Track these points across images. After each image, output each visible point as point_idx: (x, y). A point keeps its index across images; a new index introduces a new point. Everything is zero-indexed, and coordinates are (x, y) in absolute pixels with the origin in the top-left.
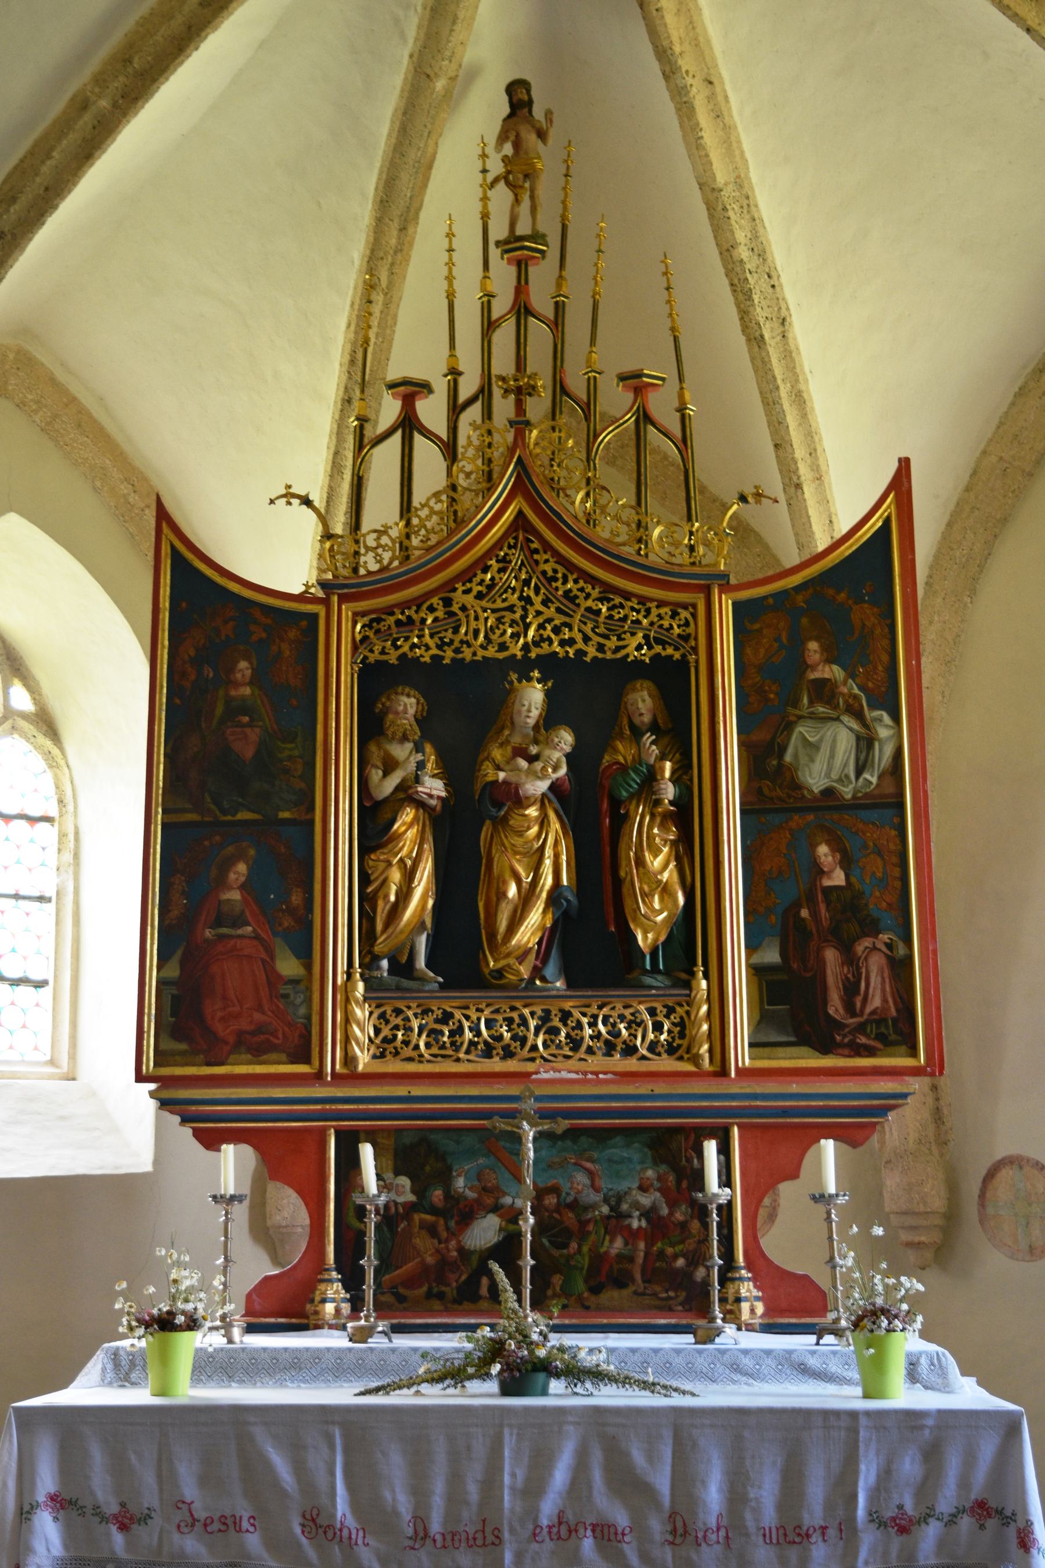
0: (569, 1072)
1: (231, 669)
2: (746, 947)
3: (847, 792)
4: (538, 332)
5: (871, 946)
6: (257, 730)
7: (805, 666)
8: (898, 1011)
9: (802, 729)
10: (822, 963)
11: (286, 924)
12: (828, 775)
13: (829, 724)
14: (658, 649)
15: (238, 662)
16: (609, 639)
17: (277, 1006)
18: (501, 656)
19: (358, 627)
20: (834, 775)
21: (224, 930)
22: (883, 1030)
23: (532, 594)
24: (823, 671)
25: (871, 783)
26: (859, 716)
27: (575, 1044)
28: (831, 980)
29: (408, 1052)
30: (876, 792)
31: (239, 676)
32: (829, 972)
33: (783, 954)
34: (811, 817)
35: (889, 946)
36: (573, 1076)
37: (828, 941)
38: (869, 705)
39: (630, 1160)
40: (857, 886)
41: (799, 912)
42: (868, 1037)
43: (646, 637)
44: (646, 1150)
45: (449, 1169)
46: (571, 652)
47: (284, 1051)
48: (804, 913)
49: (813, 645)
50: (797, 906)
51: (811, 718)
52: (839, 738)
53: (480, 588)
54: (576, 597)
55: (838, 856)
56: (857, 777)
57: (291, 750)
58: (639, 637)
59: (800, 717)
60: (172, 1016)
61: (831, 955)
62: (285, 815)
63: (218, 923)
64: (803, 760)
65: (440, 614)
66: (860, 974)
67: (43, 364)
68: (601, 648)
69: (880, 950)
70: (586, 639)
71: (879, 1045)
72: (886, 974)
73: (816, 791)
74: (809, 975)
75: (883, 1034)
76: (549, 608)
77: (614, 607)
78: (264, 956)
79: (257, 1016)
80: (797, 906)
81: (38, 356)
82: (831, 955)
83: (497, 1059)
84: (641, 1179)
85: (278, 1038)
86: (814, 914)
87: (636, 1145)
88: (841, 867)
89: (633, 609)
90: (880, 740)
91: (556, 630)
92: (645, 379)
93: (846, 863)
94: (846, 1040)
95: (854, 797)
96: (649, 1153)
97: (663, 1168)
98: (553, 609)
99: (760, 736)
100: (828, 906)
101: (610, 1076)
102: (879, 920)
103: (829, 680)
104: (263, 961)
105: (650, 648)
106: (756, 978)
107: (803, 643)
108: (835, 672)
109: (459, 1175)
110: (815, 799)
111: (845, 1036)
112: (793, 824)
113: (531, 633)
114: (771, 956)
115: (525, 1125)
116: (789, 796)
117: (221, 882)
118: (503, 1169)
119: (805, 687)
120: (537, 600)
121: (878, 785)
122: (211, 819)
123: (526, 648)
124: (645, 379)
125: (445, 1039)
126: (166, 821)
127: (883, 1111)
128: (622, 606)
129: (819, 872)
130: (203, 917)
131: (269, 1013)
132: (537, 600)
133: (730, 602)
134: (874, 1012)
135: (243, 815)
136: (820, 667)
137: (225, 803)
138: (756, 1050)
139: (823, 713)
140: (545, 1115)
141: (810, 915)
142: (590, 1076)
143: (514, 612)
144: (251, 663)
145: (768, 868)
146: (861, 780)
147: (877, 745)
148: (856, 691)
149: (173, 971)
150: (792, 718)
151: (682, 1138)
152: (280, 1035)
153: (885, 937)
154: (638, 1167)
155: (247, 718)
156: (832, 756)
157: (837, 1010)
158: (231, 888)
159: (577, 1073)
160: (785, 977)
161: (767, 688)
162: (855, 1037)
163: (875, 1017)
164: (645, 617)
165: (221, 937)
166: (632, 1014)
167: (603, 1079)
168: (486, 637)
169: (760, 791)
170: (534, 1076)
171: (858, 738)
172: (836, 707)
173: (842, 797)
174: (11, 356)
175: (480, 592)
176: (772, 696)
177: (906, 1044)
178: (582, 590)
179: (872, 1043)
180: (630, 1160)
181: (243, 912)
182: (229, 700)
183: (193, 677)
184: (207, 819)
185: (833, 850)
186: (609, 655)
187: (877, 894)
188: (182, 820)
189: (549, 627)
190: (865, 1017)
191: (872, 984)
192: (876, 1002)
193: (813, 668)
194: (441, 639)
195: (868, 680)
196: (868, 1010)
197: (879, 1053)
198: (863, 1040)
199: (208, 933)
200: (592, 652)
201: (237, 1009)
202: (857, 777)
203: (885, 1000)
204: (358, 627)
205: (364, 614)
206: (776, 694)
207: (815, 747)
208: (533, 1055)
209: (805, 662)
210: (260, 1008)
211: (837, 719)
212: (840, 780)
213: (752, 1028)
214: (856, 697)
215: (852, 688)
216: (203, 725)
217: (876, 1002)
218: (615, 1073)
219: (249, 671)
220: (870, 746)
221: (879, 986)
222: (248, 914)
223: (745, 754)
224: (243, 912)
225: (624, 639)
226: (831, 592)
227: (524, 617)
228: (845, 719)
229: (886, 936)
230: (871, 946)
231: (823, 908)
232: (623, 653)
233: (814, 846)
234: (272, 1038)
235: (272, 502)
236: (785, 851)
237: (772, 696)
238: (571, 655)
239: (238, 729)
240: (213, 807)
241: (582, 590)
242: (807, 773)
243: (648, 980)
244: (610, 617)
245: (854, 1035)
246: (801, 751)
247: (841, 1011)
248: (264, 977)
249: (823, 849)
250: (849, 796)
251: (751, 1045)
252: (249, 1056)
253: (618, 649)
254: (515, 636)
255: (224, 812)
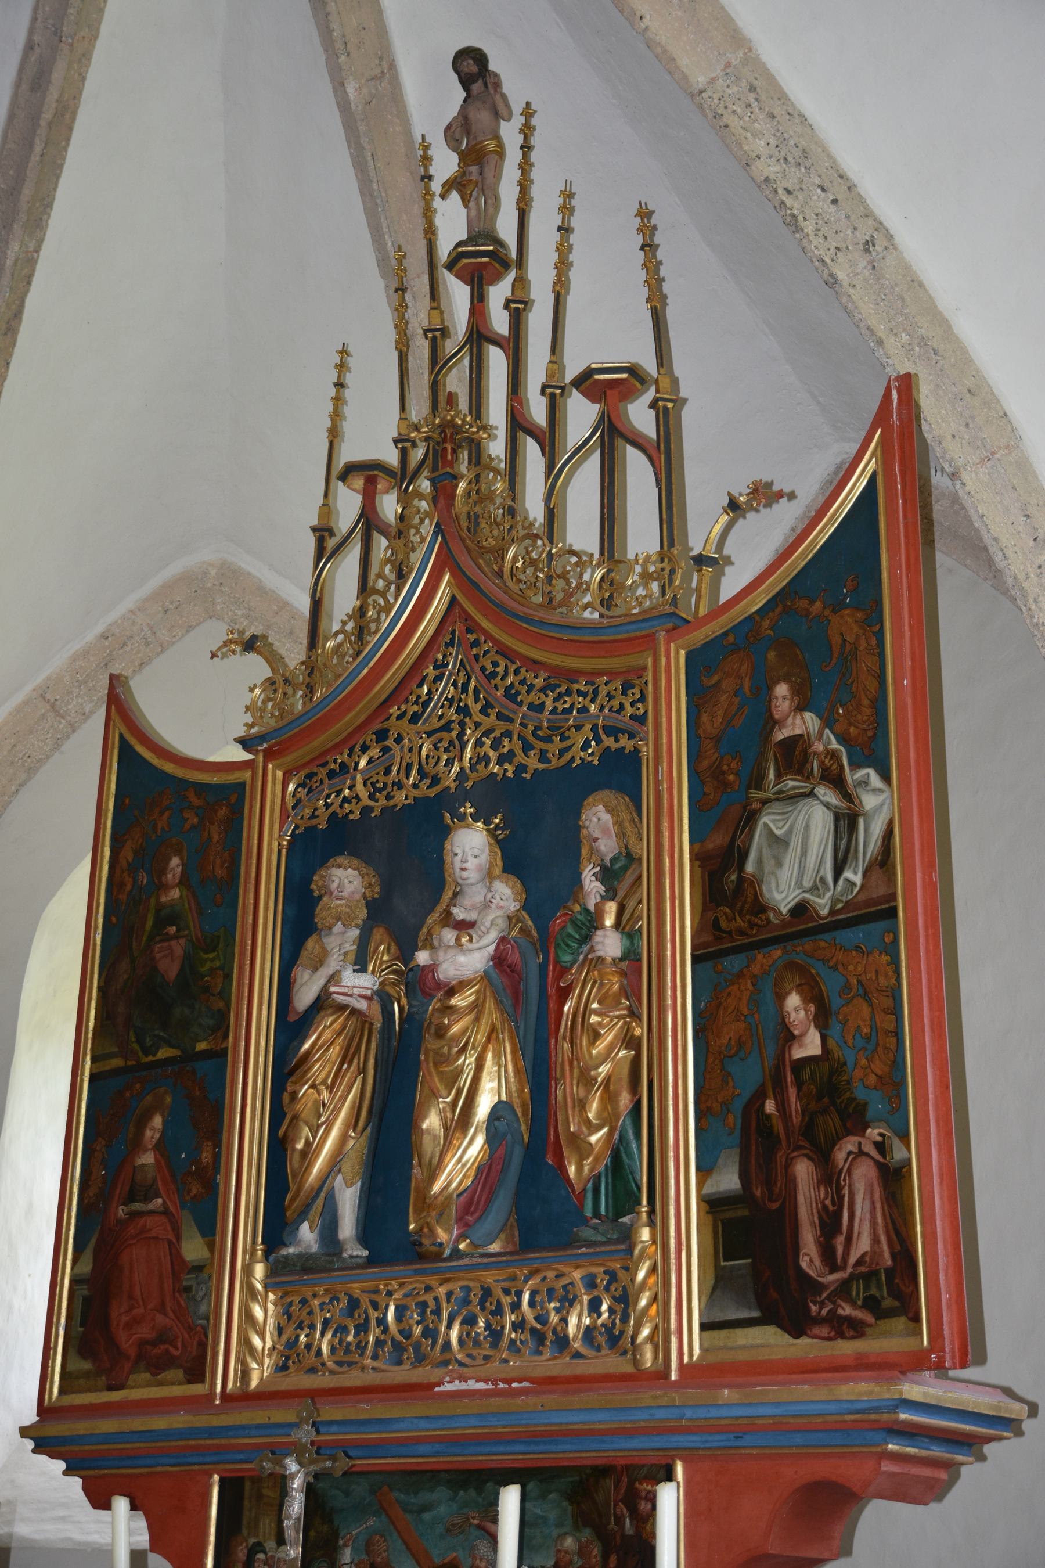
0: (478, 1381)
1: (163, 871)
2: (698, 1169)
3: (823, 904)
4: (497, 360)
5: (855, 1149)
6: (182, 941)
7: (772, 723)
8: (893, 1256)
9: (769, 820)
10: (791, 1183)
11: (194, 1191)
12: (799, 884)
13: (801, 804)
14: (609, 742)
15: (171, 859)
16: (552, 742)
17: (179, 1304)
18: (432, 793)
19: (291, 787)
20: (807, 883)
21: (137, 1206)
22: (874, 1291)
23: (470, 701)
24: (793, 724)
25: (854, 884)
26: (837, 782)
27: (495, 1334)
28: (803, 1212)
29: (311, 1359)
30: (860, 898)
31: (170, 876)
32: (801, 1199)
33: (744, 1176)
34: (777, 952)
35: (881, 1147)
36: (481, 1385)
37: (800, 1148)
38: (850, 764)
39: (545, 1519)
40: (837, 1053)
41: (763, 1104)
42: (853, 1303)
43: (594, 728)
44: (565, 1504)
45: (335, 1534)
46: (510, 769)
47: (181, 1366)
48: (770, 1106)
49: (782, 690)
50: (760, 1096)
51: (777, 799)
52: (813, 823)
53: (415, 708)
54: (518, 693)
55: (812, 1008)
56: (836, 879)
57: (212, 960)
58: (587, 731)
59: (765, 802)
60: (80, 1327)
61: (803, 1170)
62: (202, 1046)
63: (131, 1198)
64: (769, 864)
65: (375, 752)
66: (841, 1198)
67: (249, 574)
68: (543, 757)
69: (867, 1155)
70: (527, 748)
71: (869, 1318)
72: (877, 1195)
73: (784, 911)
74: (775, 1206)
75: (872, 1298)
76: (488, 716)
77: (560, 696)
78: (171, 1236)
79: (160, 1318)
80: (760, 1096)
81: (243, 566)
82: (803, 1170)
83: (406, 1366)
84: (559, 1551)
85: (177, 1349)
86: (782, 1106)
87: (553, 1496)
88: (816, 1027)
89: (580, 693)
90: (865, 815)
91: (496, 745)
92: (597, 377)
93: (822, 1018)
94: (824, 1312)
95: (833, 912)
96: (570, 1508)
97: (587, 1533)
98: (493, 717)
99: (717, 840)
100: (799, 1090)
101: (526, 1384)
102: (865, 1105)
103: (801, 736)
104: (170, 1242)
105: (599, 742)
106: (710, 1217)
107: (770, 689)
108: (808, 723)
109: (346, 1545)
110: (784, 924)
111: (822, 1305)
112: (756, 969)
113: (468, 754)
114: (728, 1180)
115: (293, 1467)
116: (752, 925)
117: (136, 1145)
118: (395, 1535)
119: (771, 756)
120: (475, 708)
121: (862, 886)
122: (134, 1063)
123: (462, 775)
124: (597, 377)
125: (350, 1338)
126: (94, 1071)
127: (970, 1444)
128: (568, 693)
129: (788, 1037)
130: (118, 1192)
131: (171, 1315)
132: (475, 708)
133: (683, 653)
134: (860, 1262)
135: (164, 1053)
136: (790, 720)
137: (148, 1040)
138: (707, 1334)
139: (794, 788)
140: (319, 1448)
141: (778, 1110)
142: (501, 1385)
143: (450, 730)
144: (181, 859)
145: (725, 1041)
146: (841, 882)
147: (861, 821)
148: (835, 745)
149: (86, 1267)
150: (756, 805)
151: (609, 1483)
152: (179, 1345)
153: (873, 1133)
154: (555, 1532)
155: (174, 928)
156: (804, 853)
157: (811, 1261)
158: (146, 1150)
159: (486, 1381)
160: (746, 1212)
161: (725, 767)
162: (837, 1307)
163: (863, 1269)
164: (592, 701)
165: (134, 1215)
166: (565, 1287)
167: (517, 1388)
168: (420, 771)
169: (716, 924)
170: (437, 1389)
171: (837, 817)
172: (808, 778)
173: (817, 913)
174: (213, 572)
175: (415, 714)
176: (731, 777)
177: (906, 1314)
178: (523, 682)
179: (859, 1314)
180: (545, 1519)
181: (155, 1180)
182: (160, 907)
183: (129, 887)
184: (129, 1063)
185: (806, 1000)
186: (555, 763)
187: (864, 1062)
188: (108, 1068)
189: (488, 742)
190: (849, 1270)
191: (858, 1213)
192: (863, 1245)
193: (780, 723)
194: (373, 784)
195: (850, 724)
196: (853, 1259)
197: (868, 1330)
198: (846, 1310)
199: (121, 1212)
200: (533, 763)
201: (141, 1310)
202: (836, 879)
203: (875, 1240)
204: (291, 787)
205: (298, 769)
206: (737, 774)
207: (779, 843)
208: (447, 1356)
209: (771, 716)
210: (162, 1309)
211: (811, 794)
212: (814, 889)
213: (704, 1299)
214: (834, 755)
215: (829, 743)
216: (134, 944)
217: (863, 1245)
218: (531, 1380)
219: (180, 869)
220: (853, 827)
221: (868, 1216)
222: (160, 1183)
223: (699, 871)
224: (155, 1180)
225: (569, 738)
226: (803, 604)
227: (462, 733)
228: (821, 791)
229: (876, 1131)
230: (855, 1149)
231: (792, 1092)
232: (568, 756)
233: (780, 998)
234: (171, 1349)
235: (214, 655)
236: (745, 1011)
237: (731, 777)
238: (510, 774)
239: (166, 944)
240: (136, 1046)
241: (523, 682)
242: (773, 885)
243: (587, 1233)
244: (554, 711)
245: (834, 1303)
246: (766, 852)
247: (818, 1262)
248: (169, 1266)
249: (794, 1000)
250: (824, 912)
251: (703, 1327)
252: (148, 1375)
253: (562, 752)
254: (449, 763)
255: (146, 1052)
